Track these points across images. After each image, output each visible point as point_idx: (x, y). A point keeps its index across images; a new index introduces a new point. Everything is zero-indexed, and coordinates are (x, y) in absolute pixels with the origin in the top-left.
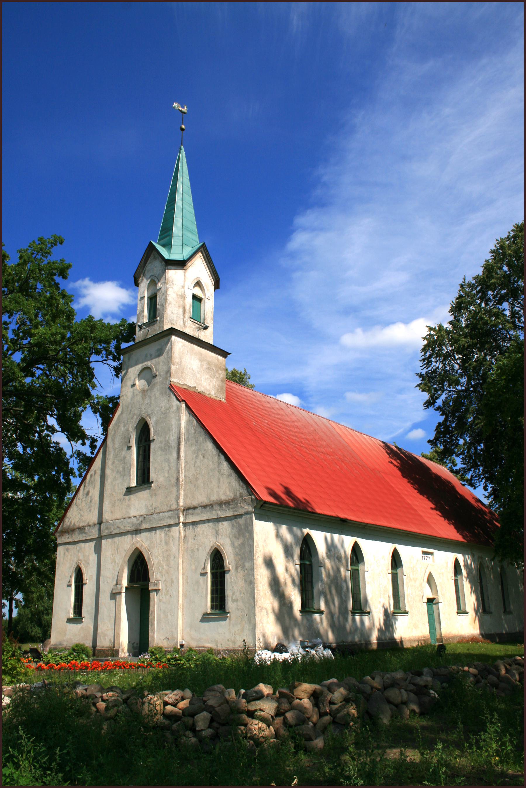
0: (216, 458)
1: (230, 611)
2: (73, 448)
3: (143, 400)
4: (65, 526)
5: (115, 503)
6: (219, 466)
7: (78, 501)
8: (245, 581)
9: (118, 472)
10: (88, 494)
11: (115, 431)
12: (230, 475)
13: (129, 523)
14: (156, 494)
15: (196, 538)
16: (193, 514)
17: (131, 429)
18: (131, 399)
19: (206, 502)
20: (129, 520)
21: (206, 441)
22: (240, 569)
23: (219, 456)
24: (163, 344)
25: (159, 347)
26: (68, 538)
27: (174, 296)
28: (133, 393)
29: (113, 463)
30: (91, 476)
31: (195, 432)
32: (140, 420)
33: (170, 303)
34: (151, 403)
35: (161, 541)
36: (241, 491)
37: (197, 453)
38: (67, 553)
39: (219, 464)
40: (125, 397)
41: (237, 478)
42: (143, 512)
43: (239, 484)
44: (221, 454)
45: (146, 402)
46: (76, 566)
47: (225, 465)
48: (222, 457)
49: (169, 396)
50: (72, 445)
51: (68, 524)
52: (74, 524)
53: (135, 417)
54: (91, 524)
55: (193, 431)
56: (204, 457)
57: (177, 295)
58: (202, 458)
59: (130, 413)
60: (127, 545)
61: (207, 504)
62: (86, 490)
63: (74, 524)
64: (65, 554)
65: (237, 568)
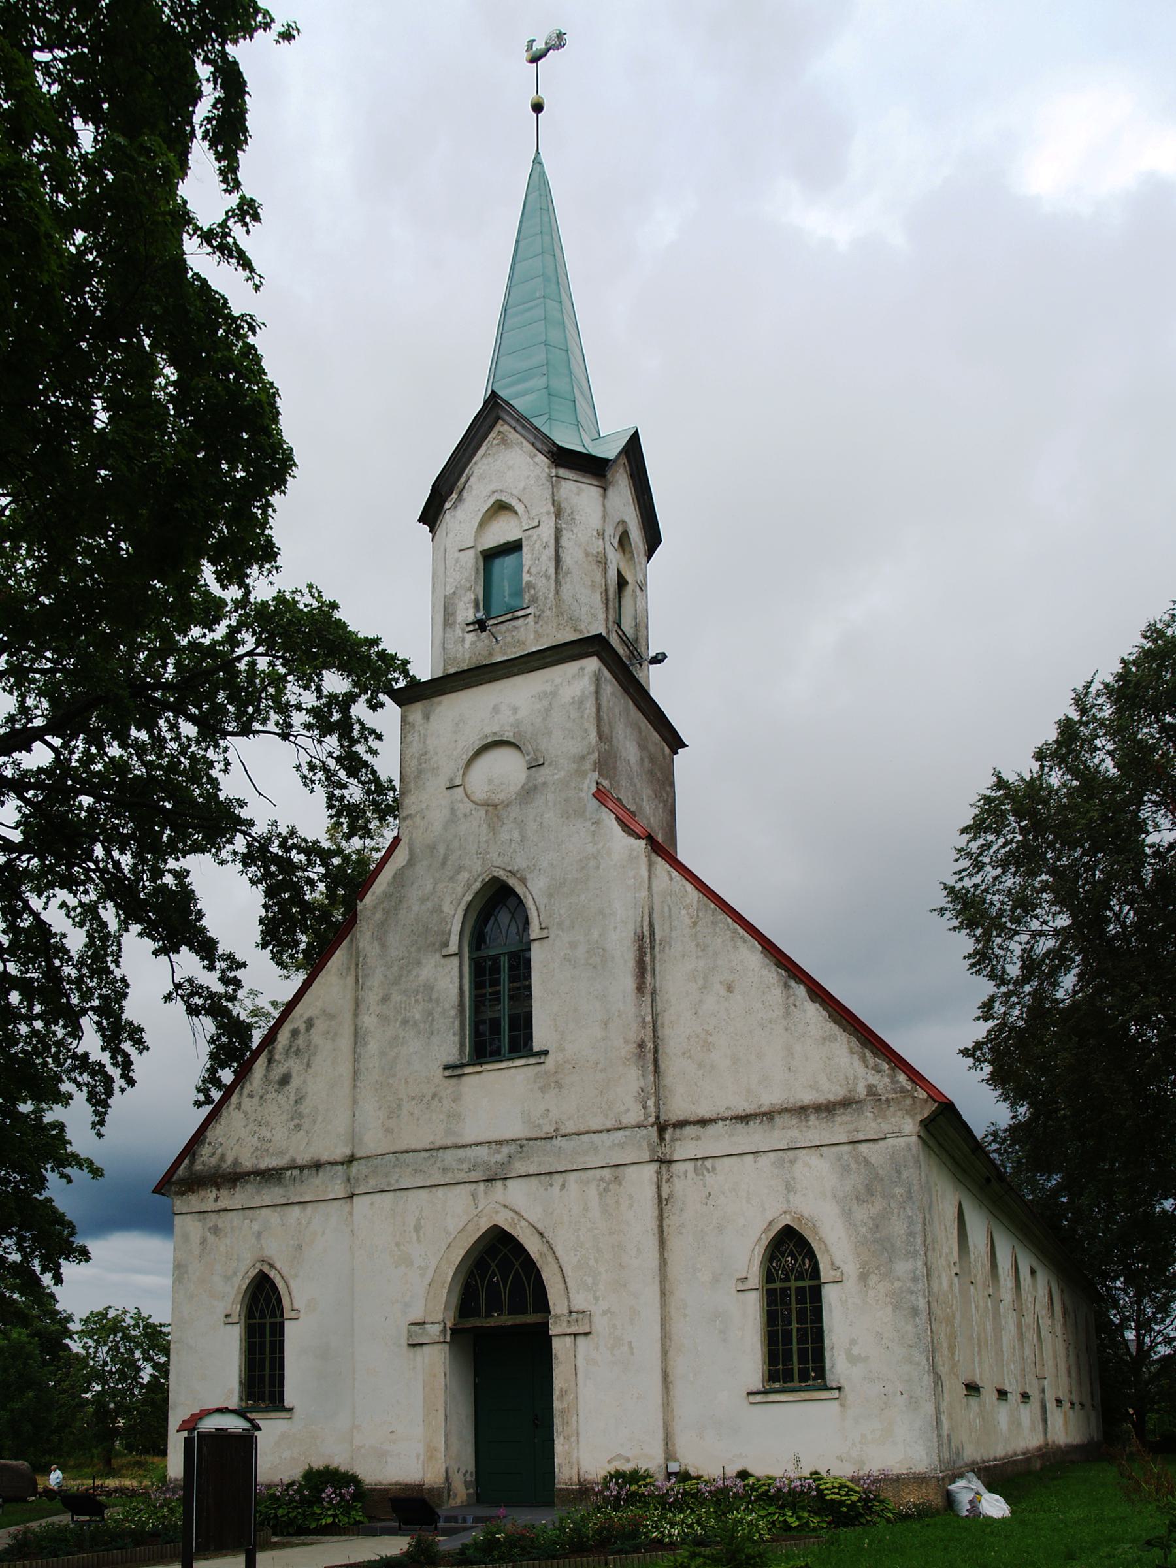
0: (777, 992)
1: (843, 1383)
2: (173, 972)
3: (493, 830)
4: (198, 1167)
5: (399, 1106)
6: (787, 1014)
7: (246, 1101)
8: (896, 1307)
9: (405, 1022)
10: (285, 1080)
11: (387, 913)
12: (832, 1038)
13: (461, 1161)
14: (559, 1085)
15: (711, 1202)
16: (698, 1138)
17: (447, 908)
18: (446, 827)
19: (743, 1106)
20: (461, 1153)
21: (736, 947)
22: (873, 1279)
23: (786, 986)
24: (558, 681)
25: (548, 688)
26: (216, 1200)
27: (580, 555)
28: (453, 811)
29: (385, 999)
30: (295, 1033)
31: (695, 924)
32: (486, 885)
33: (568, 572)
34: (523, 839)
35: (586, 1209)
36: (874, 1079)
37: (705, 979)
38: (211, 1238)
39: (787, 1007)
40: (418, 819)
41: (855, 1043)
42: (515, 1129)
43: (864, 1059)
44: (792, 983)
45: (505, 836)
46: (253, 1273)
47: (813, 1012)
48: (801, 990)
49: (597, 823)
50: (171, 962)
51: (213, 1161)
52: (236, 1162)
53: (465, 875)
54: (300, 1162)
55: (688, 921)
56: (730, 989)
57: (587, 554)
58: (723, 992)
59: (444, 863)
60: (447, 1226)
61: (749, 1112)
62: (278, 1071)
63: (236, 1162)
64: (204, 1242)
65: (863, 1277)
